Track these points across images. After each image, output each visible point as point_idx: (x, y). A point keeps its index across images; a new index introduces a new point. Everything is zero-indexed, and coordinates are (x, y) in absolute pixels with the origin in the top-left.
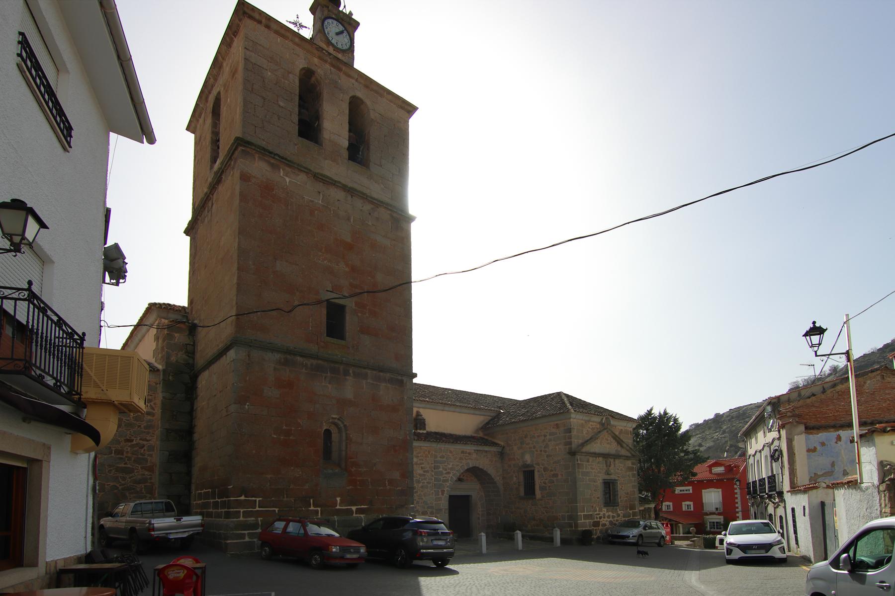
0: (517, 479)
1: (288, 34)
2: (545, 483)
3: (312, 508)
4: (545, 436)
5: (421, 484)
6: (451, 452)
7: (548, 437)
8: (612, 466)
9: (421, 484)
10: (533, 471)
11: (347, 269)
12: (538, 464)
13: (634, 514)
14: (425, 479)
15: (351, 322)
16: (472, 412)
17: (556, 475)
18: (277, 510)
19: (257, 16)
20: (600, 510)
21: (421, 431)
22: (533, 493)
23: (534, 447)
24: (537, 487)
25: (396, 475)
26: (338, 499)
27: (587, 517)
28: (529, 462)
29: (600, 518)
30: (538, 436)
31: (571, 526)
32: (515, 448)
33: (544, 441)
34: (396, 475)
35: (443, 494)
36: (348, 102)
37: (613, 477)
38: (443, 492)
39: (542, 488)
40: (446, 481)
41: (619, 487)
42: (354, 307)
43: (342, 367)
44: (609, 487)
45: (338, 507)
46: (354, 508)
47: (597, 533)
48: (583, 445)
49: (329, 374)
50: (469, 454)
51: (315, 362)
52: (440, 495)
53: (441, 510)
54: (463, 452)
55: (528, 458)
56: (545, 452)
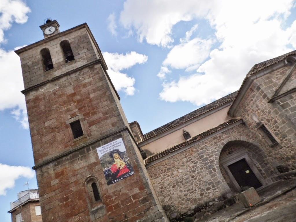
11: (76, 104)
12: (262, 120)
15: (84, 126)
16: (217, 110)
17: (276, 122)
19: (21, 51)
23: (253, 110)
25: (137, 190)
28: (257, 121)
34: (137, 190)
35: (215, 171)
38: (214, 170)
40: (213, 161)
50: (220, 137)
51: (71, 155)
52: (214, 172)
53: (219, 182)
55: (256, 119)
56: (259, 109)
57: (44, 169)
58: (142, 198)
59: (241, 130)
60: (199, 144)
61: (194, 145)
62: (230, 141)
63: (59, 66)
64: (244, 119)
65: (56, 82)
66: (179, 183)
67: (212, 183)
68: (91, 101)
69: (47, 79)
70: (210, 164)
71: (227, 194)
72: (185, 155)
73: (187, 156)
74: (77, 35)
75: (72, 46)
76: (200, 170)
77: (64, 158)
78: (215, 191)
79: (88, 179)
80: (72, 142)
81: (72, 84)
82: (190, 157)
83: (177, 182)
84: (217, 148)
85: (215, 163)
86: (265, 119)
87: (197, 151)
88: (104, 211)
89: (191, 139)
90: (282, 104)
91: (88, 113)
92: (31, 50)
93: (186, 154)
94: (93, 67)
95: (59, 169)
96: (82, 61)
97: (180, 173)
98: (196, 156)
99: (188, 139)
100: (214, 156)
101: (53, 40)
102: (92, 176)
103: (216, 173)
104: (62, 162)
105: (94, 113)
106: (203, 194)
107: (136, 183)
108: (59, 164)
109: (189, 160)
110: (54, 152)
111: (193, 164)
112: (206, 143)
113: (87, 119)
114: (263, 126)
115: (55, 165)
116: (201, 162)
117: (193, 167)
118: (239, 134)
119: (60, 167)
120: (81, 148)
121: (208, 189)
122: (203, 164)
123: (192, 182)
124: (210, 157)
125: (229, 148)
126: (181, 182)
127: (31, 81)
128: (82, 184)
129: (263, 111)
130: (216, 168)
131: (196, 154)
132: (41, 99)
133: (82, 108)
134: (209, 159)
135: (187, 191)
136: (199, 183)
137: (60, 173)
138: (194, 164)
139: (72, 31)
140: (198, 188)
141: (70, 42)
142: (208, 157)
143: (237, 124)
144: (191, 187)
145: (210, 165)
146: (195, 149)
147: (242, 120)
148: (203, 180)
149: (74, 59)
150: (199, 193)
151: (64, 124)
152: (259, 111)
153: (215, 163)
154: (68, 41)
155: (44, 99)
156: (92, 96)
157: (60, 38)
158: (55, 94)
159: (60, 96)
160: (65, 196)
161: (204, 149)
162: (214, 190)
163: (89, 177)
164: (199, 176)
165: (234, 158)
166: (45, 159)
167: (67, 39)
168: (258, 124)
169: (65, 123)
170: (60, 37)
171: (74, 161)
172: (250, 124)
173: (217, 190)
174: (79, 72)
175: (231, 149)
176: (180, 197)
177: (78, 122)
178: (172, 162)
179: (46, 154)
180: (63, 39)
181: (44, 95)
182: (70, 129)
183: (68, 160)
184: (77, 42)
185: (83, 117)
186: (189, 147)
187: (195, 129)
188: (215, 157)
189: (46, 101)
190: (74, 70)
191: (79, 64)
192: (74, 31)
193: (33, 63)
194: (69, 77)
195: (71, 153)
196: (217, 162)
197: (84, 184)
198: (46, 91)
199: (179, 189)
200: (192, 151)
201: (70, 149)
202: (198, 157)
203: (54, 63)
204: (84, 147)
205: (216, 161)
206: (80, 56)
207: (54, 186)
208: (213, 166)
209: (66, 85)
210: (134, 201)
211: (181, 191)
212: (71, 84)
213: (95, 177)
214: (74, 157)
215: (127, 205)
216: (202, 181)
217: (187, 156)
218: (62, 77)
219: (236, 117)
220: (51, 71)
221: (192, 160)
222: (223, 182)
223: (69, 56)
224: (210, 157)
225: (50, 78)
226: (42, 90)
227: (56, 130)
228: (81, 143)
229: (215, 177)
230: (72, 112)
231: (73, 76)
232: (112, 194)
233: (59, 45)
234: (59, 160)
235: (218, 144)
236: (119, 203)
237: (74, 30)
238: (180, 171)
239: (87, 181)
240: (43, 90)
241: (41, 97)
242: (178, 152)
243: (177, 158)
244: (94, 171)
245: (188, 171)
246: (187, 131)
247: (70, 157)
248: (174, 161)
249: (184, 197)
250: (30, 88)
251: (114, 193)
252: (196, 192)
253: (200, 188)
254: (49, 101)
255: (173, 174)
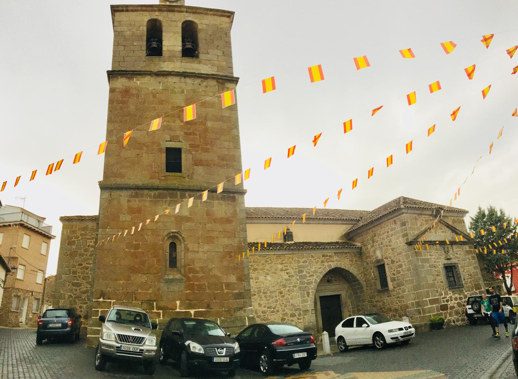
0: (374, 273)
2: (394, 275)
3: (155, 311)
4: (388, 232)
7: (390, 233)
8: (451, 252)
10: (384, 265)
13: (481, 292)
14: (291, 283)
15: (186, 159)
16: (335, 222)
17: (400, 266)
20: (446, 294)
21: (289, 243)
22: (387, 285)
23: (382, 243)
24: (389, 279)
25: (233, 279)
26: (178, 303)
27: (432, 302)
29: (447, 301)
30: (383, 234)
31: (420, 313)
32: (369, 246)
33: (388, 236)
34: (233, 279)
35: (308, 296)
36: (180, 30)
37: (453, 261)
38: (308, 294)
39: (393, 280)
41: (461, 270)
42: (188, 148)
43: (179, 193)
44: (451, 270)
45: (178, 310)
47: (450, 318)
48: (418, 236)
49: (169, 199)
50: (330, 256)
51: (157, 192)
55: (379, 254)
56: (390, 246)
57: (116, 193)
58: (237, 291)
59: (354, 259)
60: (305, 254)
61: (297, 253)
62: (339, 266)
63: (171, 58)
64: (364, 248)
65: (161, 79)
66: (262, 294)
67: (299, 309)
68: (206, 130)
69: (148, 69)
70: (306, 285)
71: (466, 325)
72: (282, 261)
73: (284, 262)
74: (213, 22)
75: (201, 36)
76: (292, 288)
77: (146, 192)
78: (300, 321)
79: (171, 234)
80: (163, 175)
81: (185, 92)
82: (287, 266)
83: (259, 292)
84: (322, 269)
85: (312, 286)
86: (390, 258)
87: (299, 262)
88: (182, 286)
89: (292, 242)
90: (417, 250)
91: (198, 146)
92: (134, 13)
93: (284, 260)
94: (223, 84)
95: (136, 203)
96: (210, 65)
97: (268, 282)
98: (294, 268)
99: (289, 241)
100: (315, 277)
101: (173, 11)
102: (177, 233)
103: (309, 299)
104: (142, 195)
105: (206, 151)
106: (285, 319)
107: (235, 269)
108: (137, 196)
109: (284, 268)
110: (136, 177)
111: (286, 277)
112: (312, 257)
113: (193, 153)
114: (383, 265)
115: (132, 196)
116: (298, 278)
117: (286, 280)
118: (351, 263)
119: (137, 201)
120: (174, 189)
121: (293, 315)
122: (299, 282)
123: (277, 298)
124: (309, 277)
125: (336, 274)
126: (264, 293)
127: (124, 61)
128: (161, 238)
129: (393, 249)
130: (311, 293)
131: (296, 265)
132: (133, 95)
133: (190, 134)
134: (308, 278)
135: (268, 308)
136: (285, 303)
137: (135, 208)
138: (289, 276)
139: (209, 12)
140: (282, 309)
141: (200, 27)
142: (308, 275)
143: (354, 251)
144: (273, 305)
145: (306, 287)
146: (296, 258)
147: (361, 248)
148: (291, 301)
149: (197, 57)
150: (281, 316)
151: (158, 146)
152: (389, 248)
153: (312, 286)
154: (197, 24)
155: (138, 96)
156: (209, 124)
157: (187, 14)
158: (154, 96)
159: (161, 102)
160: (134, 243)
161: (307, 264)
162: (298, 319)
163: (172, 232)
164: (289, 295)
165: (330, 290)
166: (119, 181)
167: (196, 21)
168: (378, 261)
169: (159, 144)
170: (187, 12)
171: (158, 201)
172: (367, 258)
173: (301, 321)
174: (202, 79)
175: (332, 277)
176: (256, 313)
177: (178, 151)
178: (263, 262)
179: (122, 176)
180: (190, 17)
181: (139, 90)
182: (164, 155)
183: (150, 196)
184: (210, 32)
185: (188, 148)
186: (290, 253)
187: (302, 234)
188: (315, 280)
189: (140, 100)
190: (194, 73)
191: (204, 69)
192: (211, 15)
193: (133, 34)
194: (183, 79)
195: (157, 189)
196: (314, 285)
197: (164, 238)
198: (144, 86)
199: (259, 302)
200: (292, 259)
201: (156, 182)
202: (297, 270)
203: (164, 49)
204: (178, 189)
205: (314, 284)
206: (209, 57)
207: (123, 222)
208: (309, 289)
209: (176, 89)
210: (226, 291)
211: (260, 305)
212: (183, 92)
213: (181, 236)
214: (159, 196)
215: (216, 292)
216: (289, 302)
217: (284, 262)
218: (173, 75)
219: (354, 241)
220: (156, 59)
221: (288, 271)
222: (312, 314)
223: (190, 50)
224: (309, 277)
225: (155, 69)
226: (138, 82)
227: (145, 148)
228: (174, 180)
229: (305, 304)
230: (173, 133)
231: (189, 81)
232: (198, 269)
233: (180, 24)
234: (138, 191)
235: (326, 264)
236: (205, 284)
237: (212, 13)
238: (269, 278)
239: (169, 235)
240: (138, 82)
241: (134, 92)
242: (276, 253)
243: (271, 260)
244: (183, 227)
245: (278, 283)
246: (291, 230)
247: (155, 194)
248: (267, 261)
249: (260, 314)
250: (122, 71)
251: (202, 268)
252: (278, 313)
253: (284, 311)
254: (144, 102)
255: (258, 278)
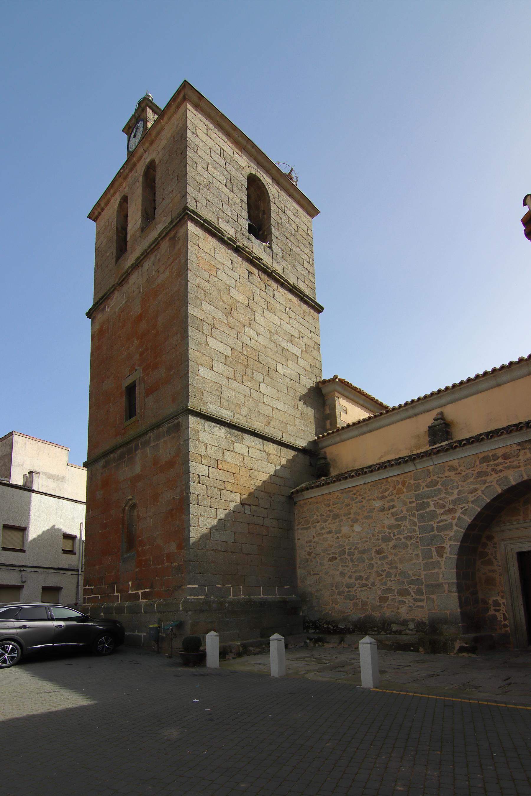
1: (249, 147)
3: (116, 594)
5: (391, 544)
6: (452, 469)
9: (391, 544)
18: (99, 596)
25: (173, 547)
26: (130, 583)
38: (440, 551)
40: (449, 527)
45: (130, 592)
46: (140, 592)
52: (436, 558)
53: (439, 586)
54: (485, 459)
